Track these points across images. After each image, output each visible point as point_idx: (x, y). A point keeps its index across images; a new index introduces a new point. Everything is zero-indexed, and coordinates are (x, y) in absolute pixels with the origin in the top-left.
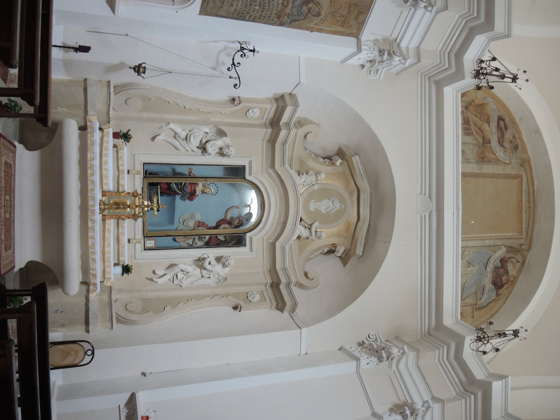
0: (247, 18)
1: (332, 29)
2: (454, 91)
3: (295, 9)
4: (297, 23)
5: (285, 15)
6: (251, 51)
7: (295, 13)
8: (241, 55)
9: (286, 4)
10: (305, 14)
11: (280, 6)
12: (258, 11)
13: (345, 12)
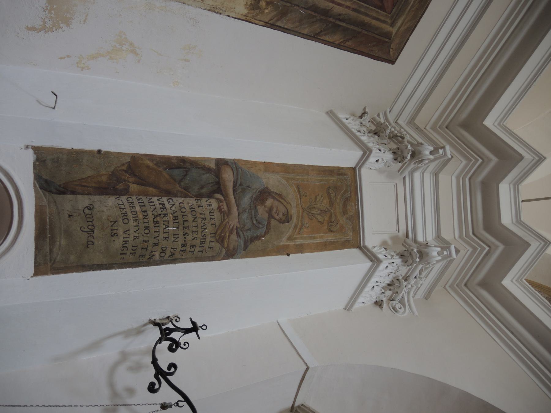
0: (157, 257)
1: (318, 240)
2: (514, 281)
3: (245, 216)
4: (257, 243)
5: (231, 233)
6: (187, 331)
7: (249, 225)
8: (171, 349)
9: (225, 208)
10: (265, 222)
11: (217, 215)
12: (176, 235)
13: (325, 204)
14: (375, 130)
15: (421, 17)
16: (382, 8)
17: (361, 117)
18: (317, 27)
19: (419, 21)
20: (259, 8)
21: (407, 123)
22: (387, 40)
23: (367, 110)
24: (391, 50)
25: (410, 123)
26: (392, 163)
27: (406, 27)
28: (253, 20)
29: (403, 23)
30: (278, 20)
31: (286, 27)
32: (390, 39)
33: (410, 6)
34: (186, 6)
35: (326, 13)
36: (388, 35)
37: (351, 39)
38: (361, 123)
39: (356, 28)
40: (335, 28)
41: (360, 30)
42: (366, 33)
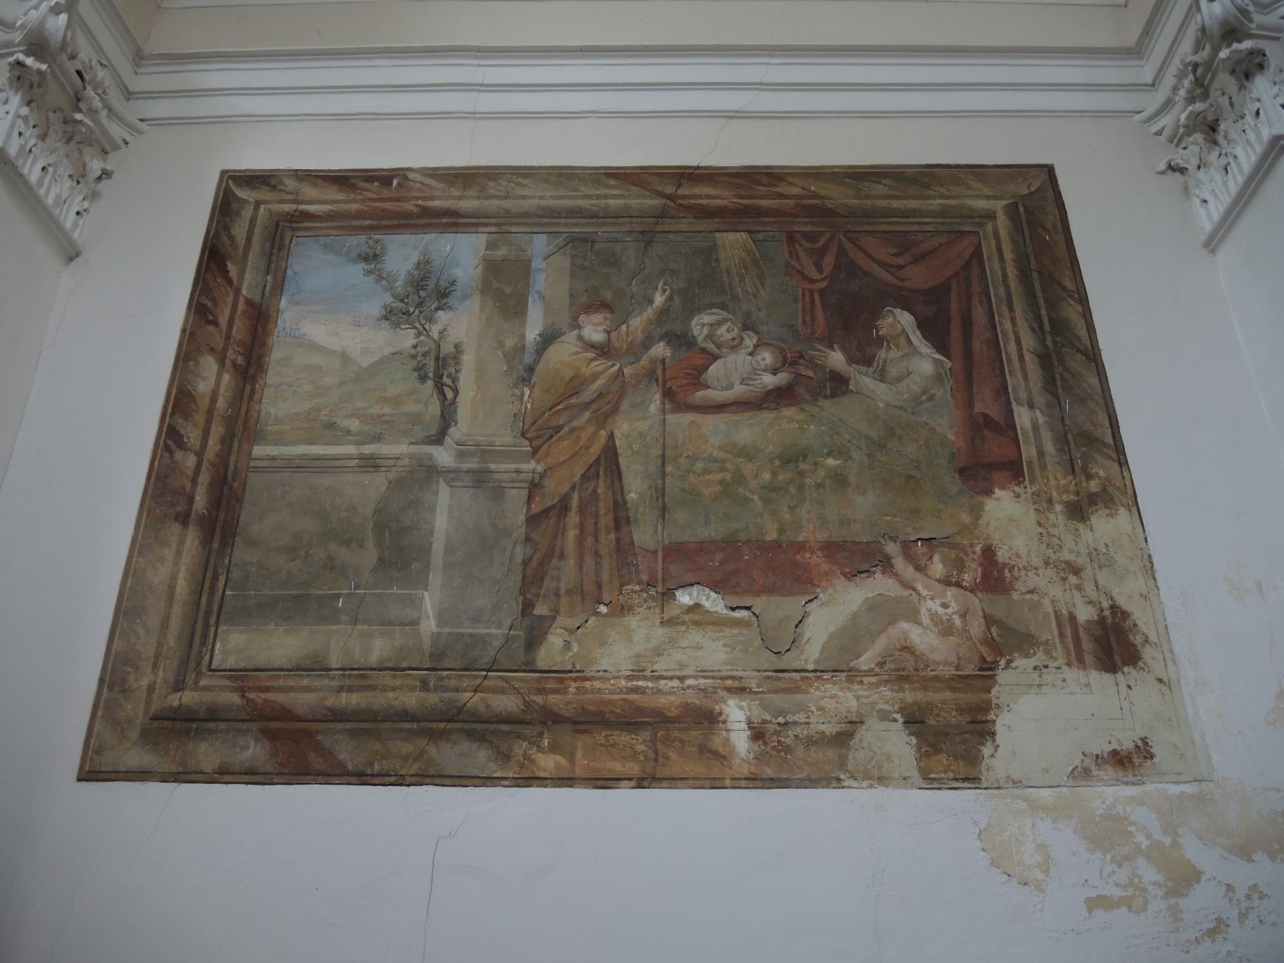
14: (1202, 132)
15: (949, 166)
16: (978, 254)
17: (1182, 170)
18: (1076, 363)
19: (957, 166)
20: (1104, 490)
21: (1142, 59)
22: (1021, 209)
23: (1163, 166)
24: (1033, 189)
25: (1139, 53)
26: (1272, 68)
27: (978, 185)
28: (1130, 492)
29: (978, 197)
30: (1105, 445)
31: (1107, 424)
32: (1016, 204)
33: (947, 202)
34: (1169, 622)
35: (1045, 360)
36: (1012, 211)
37: (1059, 283)
38: (1199, 167)
39: (1037, 285)
40: (1059, 326)
41: (1035, 275)
42: (1033, 260)
